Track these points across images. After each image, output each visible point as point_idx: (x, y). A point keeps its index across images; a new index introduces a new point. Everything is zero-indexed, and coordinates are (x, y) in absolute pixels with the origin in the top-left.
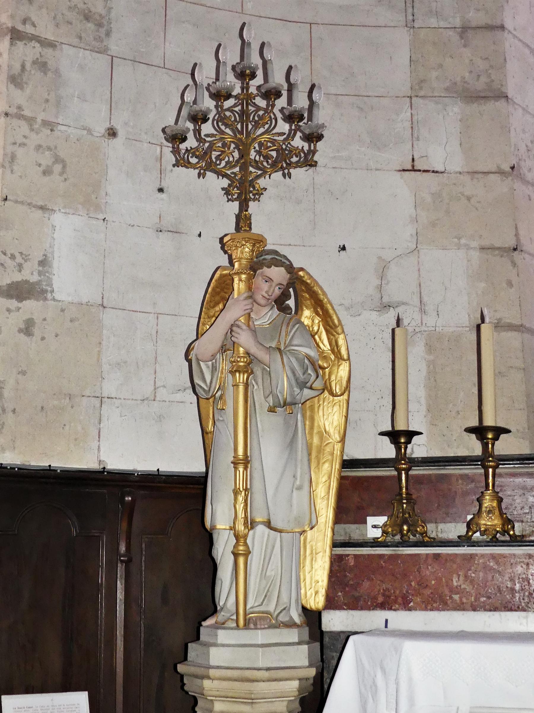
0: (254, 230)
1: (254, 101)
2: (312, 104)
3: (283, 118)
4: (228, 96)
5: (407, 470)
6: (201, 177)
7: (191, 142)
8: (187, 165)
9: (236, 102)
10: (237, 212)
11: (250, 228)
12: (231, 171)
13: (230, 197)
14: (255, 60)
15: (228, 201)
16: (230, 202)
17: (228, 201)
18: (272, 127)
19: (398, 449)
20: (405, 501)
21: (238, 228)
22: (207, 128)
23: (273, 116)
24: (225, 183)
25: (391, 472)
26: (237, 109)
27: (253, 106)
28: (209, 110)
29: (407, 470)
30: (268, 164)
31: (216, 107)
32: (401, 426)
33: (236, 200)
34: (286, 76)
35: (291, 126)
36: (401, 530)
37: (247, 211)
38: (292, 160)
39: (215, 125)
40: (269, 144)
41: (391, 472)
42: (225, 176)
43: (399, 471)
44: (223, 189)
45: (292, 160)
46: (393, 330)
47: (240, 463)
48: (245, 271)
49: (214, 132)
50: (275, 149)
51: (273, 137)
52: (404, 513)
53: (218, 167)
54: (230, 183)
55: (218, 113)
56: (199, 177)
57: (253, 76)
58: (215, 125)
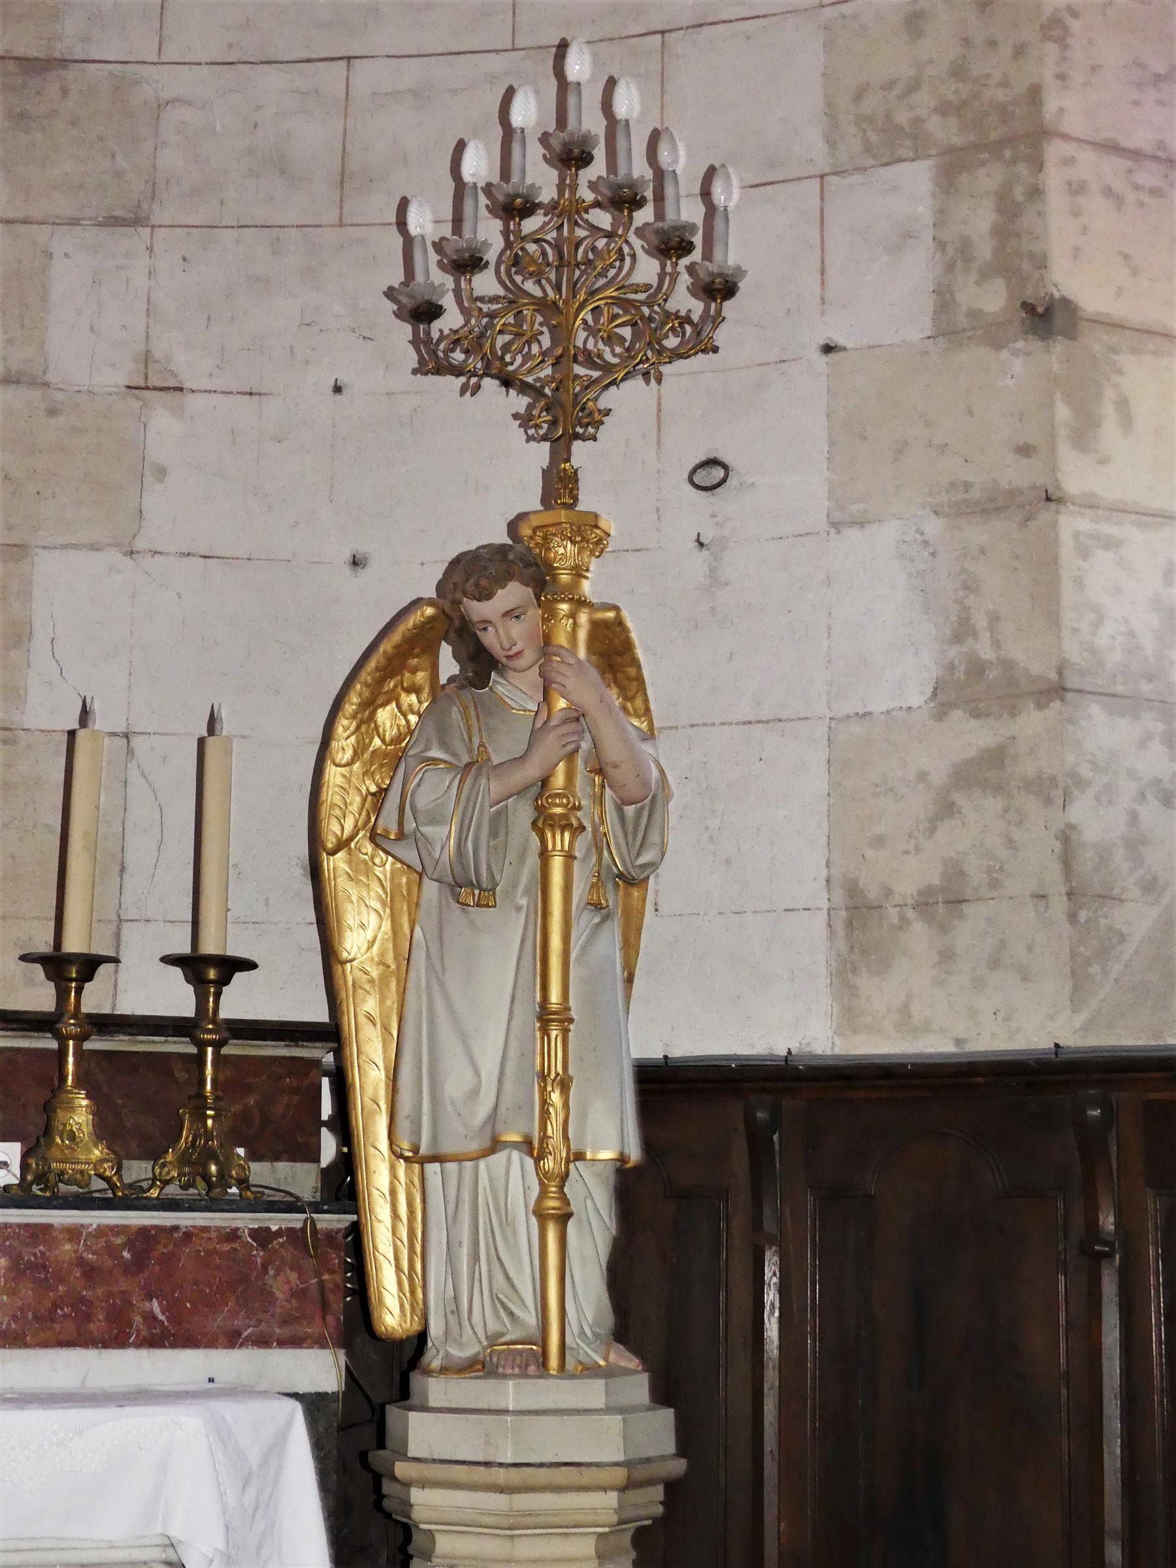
0: (581, 507)
1: (585, 216)
2: (711, 210)
3: (646, 247)
4: (528, 209)
5: (218, 1045)
6: (469, 393)
7: (451, 320)
8: (443, 368)
9: (547, 219)
10: (545, 464)
11: (576, 499)
12: (534, 377)
13: (531, 432)
14: (592, 123)
15: (527, 441)
16: (533, 444)
17: (527, 441)
18: (621, 276)
19: (62, 995)
20: (209, 1112)
21: (547, 500)
22: (485, 283)
23: (626, 249)
24: (520, 402)
25: (182, 1046)
26: (552, 236)
27: (583, 228)
28: (692, 228)
29: (218, 1045)
30: (614, 355)
31: (506, 233)
32: (210, 946)
33: (544, 438)
34: (452, 172)
35: (663, 267)
36: (206, 1177)
37: (568, 460)
38: (665, 343)
39: (503, 275)
40: (617, 310)
41: (182, 1046)
42: (525, 388)
43: (202, 1045)
44: (516, 416)
45: (665, 343)
46: (201, 742)
47: (553, 1020)
48: (563, 596)
49: (501, 292)
50: (627, 321)
51: (625, 294)
52: (208, 1135)
53: (510, 368)
54: (531, 401)
55: (508, 245)
56: (462, 393)
57: (585, 159)
58: (503, 275)
